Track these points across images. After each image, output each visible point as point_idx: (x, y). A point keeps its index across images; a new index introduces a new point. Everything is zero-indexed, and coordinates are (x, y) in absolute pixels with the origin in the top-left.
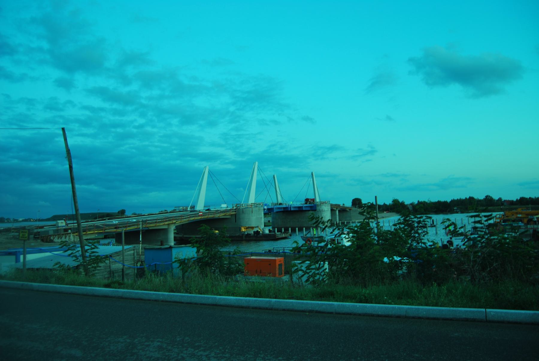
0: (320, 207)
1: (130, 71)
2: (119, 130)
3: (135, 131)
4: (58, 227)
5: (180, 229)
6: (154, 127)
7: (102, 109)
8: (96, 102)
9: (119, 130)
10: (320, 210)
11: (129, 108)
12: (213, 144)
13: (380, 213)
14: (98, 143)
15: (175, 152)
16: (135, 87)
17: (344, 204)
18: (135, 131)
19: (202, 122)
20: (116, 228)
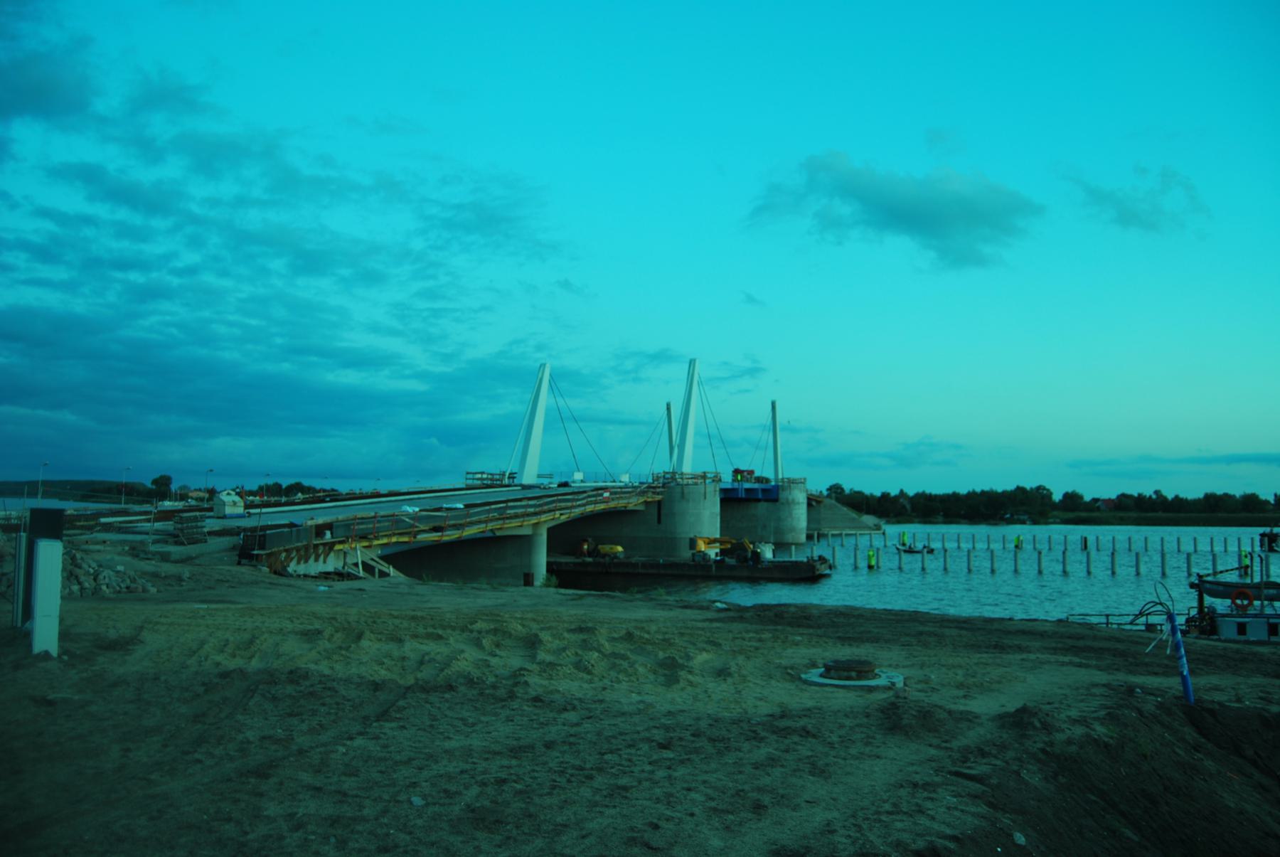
0: (788, 492)
1: (160, 126)
2: (135, 277)
3: (175, 281)
4: (224, 517)
5: (561, 538)
6: (224, 273)
7: (88, 220)
8: (72, 200)
9: (135, 277)
10: (787, 499)
11: (159, 223)
12: (375, 328)
13: (45, 498)
14: (79, 305)
15: (279, 341)
16: (172, 170)
17: (361, 489)
18: (175, 281)
19: (345, 272)
20: (435, 529)
